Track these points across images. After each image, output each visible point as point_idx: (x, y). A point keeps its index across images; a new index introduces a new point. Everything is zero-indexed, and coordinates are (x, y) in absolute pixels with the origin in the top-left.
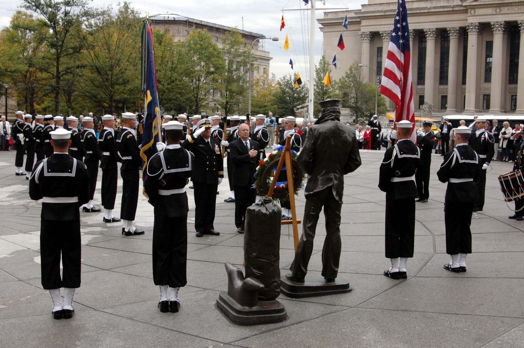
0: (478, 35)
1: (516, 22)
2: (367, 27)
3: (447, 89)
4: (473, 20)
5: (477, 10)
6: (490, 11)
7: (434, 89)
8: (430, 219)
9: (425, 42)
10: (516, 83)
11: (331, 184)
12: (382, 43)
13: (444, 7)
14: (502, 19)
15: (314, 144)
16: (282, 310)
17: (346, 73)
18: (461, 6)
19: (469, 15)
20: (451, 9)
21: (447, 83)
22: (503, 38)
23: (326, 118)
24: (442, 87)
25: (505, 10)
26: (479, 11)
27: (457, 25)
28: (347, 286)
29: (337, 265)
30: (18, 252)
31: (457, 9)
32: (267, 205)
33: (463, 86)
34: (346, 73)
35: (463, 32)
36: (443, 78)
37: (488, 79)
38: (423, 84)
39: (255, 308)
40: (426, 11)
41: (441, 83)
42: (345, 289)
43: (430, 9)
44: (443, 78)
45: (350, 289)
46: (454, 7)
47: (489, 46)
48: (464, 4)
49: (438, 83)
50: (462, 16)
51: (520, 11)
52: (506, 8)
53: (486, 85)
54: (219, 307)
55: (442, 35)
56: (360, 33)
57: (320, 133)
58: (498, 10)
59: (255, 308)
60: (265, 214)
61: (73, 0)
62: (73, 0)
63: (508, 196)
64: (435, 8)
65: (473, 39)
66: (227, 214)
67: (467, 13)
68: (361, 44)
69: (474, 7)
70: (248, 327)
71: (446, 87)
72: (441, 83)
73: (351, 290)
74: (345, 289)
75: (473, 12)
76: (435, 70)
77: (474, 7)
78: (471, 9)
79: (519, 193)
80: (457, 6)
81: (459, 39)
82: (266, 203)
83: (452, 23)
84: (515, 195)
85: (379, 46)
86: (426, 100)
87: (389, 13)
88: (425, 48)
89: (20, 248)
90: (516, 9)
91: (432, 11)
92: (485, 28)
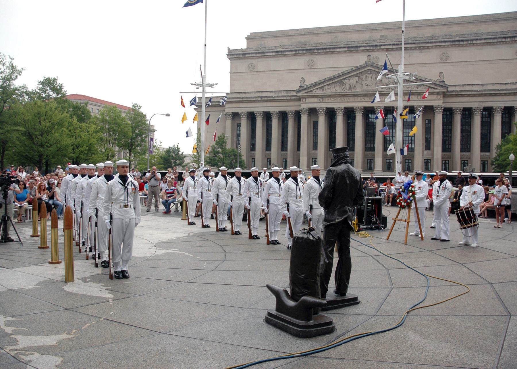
0: (308, 117)
1: (333, 108)
2: (230, 109)
3: (287, 154)
4: (305, 106)
5: (307, 99)
6: (315, 100)
7: (278, 153)
8: (8, 254)
9: (271, 121)
10: (354, 150)
11: (346, 216)
12: (241, 120)
13: (284, 96)
14: (324, 106)
15: (334, 183)
16: (330, 323)
17: (174, 146)
18: (296, 96)
19: (302, 102)
20: (289, 98)
21: (286, 150)
22: (325, 119)
23: (340, 162)
24: (283, 152)
25: (326, 100)
26: (308, 100)
27: (294, 109)
28: (356, 299)
29: (348, 283)
30: (43, 282)
31: (293, 98)
32: (312, 233)
33: (298, 152)
34: (174, 146)
35: (298, 115)
36: (284, 146)
37: (315, 146)
38: (270, 150)
39: (311, 322)
40: (272, 99)
41: (282, 150)
42: (354, 301)
43: (275, 97)
44: (284, 146)
45: (358, 301)
46: (291, 96)
47: (316, 124)
48: (298, 95)
49: (280, 149)
50: (297, 103)
51: (341, 101)
52: (327, 99)
53: (314, 152)
54: (268, 321)
55: (283, 116)
56: (224, 113)
57: (338, 174)
58: (321, 100)
59: (311, 322)
60: (312, 240)
61: (1, 73)
62: (1, 73)
63: (463, 225)
64: (278, 96)
65: (304, 119)
66: (198, 245)
67: (300, 101)
68: (225, 122)
69: (305, 97)
70: (314, 339)
71: (286, 152)
72: (282, 150)
73: (358, 303)
74: (354, 301)
75: (304, 100)
76: (278, 140)
77: (305, 97)
78: (303, 98)
79: (471, 223)
80: (293, 96)
81: (295, 119)
82: (311, 231)
83: (290, 108)
84: (469, 223)
85: (238, 122)
86: (272, 162)
87: (245, 100)
88: (271, 125)
89: (43, 279)
90: (333, 99)
91: (276, 98)
92: (313, 112)
